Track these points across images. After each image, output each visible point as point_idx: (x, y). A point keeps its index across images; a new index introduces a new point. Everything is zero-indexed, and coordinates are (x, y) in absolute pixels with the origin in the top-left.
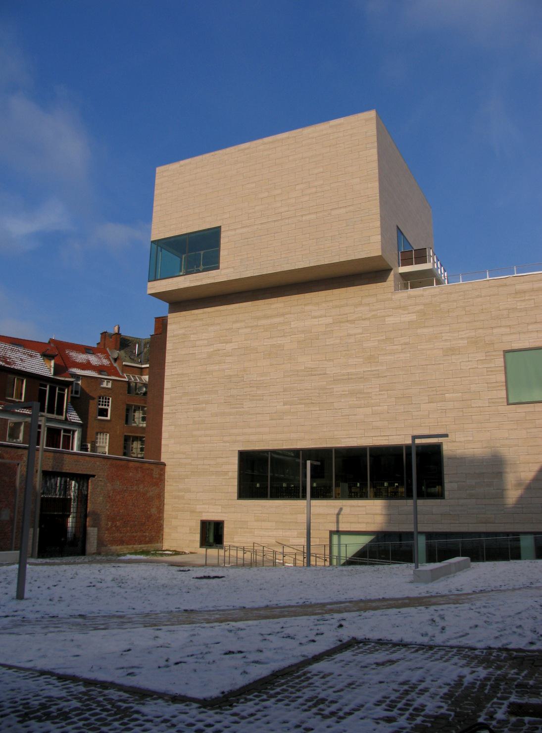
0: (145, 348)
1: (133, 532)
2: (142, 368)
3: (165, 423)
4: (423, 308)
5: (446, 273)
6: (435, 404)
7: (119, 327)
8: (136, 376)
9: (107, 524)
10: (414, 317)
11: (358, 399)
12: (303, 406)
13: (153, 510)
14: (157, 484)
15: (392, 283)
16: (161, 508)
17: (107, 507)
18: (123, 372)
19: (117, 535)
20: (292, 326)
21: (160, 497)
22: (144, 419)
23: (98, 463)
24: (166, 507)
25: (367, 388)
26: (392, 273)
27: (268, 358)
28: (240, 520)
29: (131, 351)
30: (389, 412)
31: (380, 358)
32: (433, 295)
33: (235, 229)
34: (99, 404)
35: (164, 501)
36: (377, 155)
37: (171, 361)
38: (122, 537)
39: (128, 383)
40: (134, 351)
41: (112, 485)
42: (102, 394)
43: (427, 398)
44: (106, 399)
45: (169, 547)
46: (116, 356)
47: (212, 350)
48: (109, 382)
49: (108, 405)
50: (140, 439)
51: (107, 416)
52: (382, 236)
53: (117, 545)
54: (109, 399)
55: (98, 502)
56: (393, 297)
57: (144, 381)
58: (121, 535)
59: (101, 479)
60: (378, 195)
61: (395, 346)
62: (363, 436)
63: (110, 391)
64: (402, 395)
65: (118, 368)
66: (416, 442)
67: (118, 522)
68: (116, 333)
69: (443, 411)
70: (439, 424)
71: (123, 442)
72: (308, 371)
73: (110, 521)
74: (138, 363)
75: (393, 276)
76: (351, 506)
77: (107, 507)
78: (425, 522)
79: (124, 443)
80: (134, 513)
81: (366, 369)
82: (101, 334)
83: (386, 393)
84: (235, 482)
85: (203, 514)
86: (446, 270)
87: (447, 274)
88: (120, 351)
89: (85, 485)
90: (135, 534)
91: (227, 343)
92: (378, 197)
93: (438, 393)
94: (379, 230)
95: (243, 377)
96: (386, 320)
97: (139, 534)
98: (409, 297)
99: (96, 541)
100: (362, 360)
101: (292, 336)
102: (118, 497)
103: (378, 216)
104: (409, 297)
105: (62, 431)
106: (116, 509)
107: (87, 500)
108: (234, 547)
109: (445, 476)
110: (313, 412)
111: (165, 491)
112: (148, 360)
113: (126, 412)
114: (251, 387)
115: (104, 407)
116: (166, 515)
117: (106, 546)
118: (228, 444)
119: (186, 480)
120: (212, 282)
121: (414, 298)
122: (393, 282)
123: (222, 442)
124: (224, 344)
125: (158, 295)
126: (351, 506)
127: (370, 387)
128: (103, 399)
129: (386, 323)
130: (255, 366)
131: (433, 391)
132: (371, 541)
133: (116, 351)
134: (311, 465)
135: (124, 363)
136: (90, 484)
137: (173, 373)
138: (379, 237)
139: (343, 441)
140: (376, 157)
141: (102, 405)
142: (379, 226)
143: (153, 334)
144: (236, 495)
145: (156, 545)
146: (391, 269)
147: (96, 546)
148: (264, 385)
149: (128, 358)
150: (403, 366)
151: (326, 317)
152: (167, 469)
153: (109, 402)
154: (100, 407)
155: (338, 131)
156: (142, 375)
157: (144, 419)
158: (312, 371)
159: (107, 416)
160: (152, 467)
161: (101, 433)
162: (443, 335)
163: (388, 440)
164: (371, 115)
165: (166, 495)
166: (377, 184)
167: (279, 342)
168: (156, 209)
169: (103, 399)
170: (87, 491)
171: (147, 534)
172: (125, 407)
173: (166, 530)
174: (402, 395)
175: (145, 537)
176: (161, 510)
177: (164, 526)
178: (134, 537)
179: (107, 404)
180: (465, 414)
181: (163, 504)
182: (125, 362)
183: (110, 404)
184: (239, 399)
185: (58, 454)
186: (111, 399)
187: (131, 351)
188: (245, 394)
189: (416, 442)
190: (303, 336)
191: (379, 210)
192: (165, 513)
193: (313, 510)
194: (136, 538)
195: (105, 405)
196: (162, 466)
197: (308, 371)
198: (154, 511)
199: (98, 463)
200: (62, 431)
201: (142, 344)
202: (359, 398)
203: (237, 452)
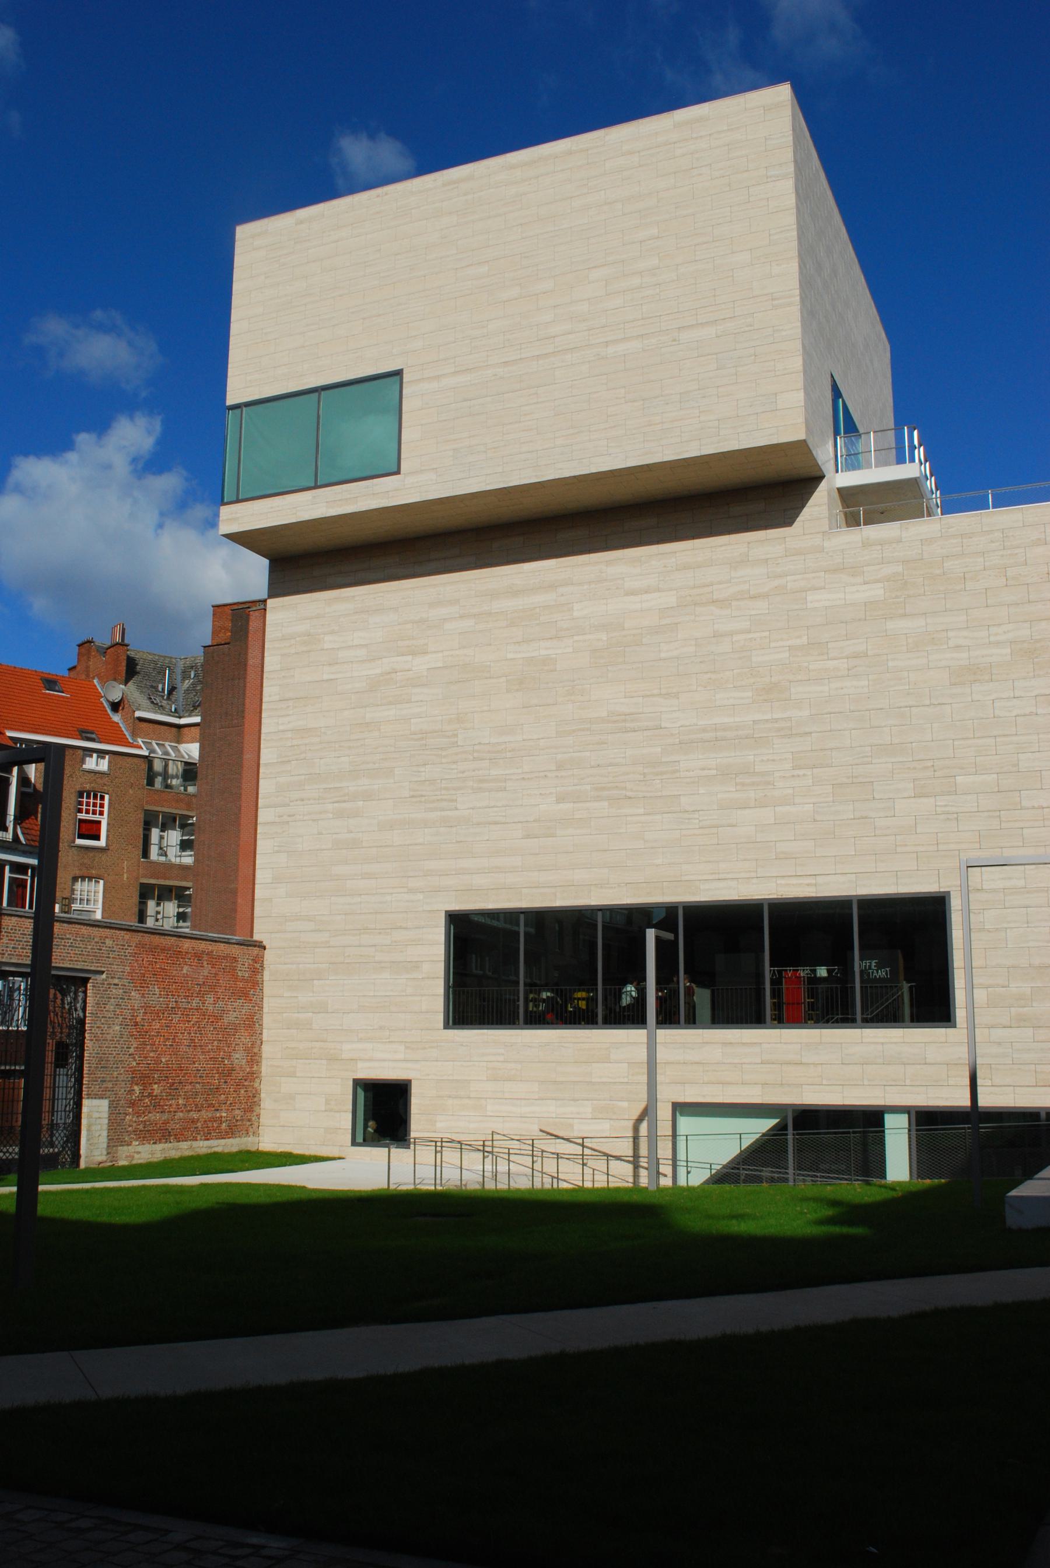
0: (184, 679)
1: (189, 1111)
2: (179, 727)
3: (264, 846)
4: (900, 569)
5: (938, 492)
6: (932, 800)
7: (124, 630)
8: (167, 744)
9: (131, 1092)
10: (877, 592)
11: (738, 788)
12: (606, 804)
13: (237, 1056)
14: (244, 994)
15: (824, 511)
16: (256, 1050)
17: (132, 1050)
18: (134, 735)
19: (155, 1117)
20: (576, 614)
21: (252, 1023)
22: (185, 845)
23: (109, 942)
24: (267, 1050)
25: (762, 761)
26: (823, 485)
27: (517, 690)
28: (451, 1078)
29: (152, 687)
30: (818, 818)
31: (793, 690)
32: (926, 540)
33: (438, 378)
34: (80, 811)
35: (261, 1034)
36: (794, 195)
37: (277, 698)
38: (166, 1123)
39: (149, 760)
40: (160, 687)
41: (143, 996)
42: (88, 787)
43: (912, 785)
44: (95, 797)
45: (276, 1145)
46: (116, 695)
47: (378, 671)
48: (104, 758)
49: (101, 813)
50: (179, 895)
51: (97, 837)
52: (805, 392)
53: (155, 1143)
54: (102, 798)
55: (109, 1037)
56: (826, 544)
57: (187, 757)
58: (165, 1116)
59: (116, 981)
60: (797, 292)
61: (830, 662)
62: (753, 875)
63: (106, 780)
64: (848, 778)
65: (121, 725)
66: (648, 931)
67: (156, 1086)
68: (117, 644)
69: (950, 816)
70: (941, 847)
71: (136, 899)
72: (615, 722)
73: (137, 1084)
74: (170, 714)
75: (826, 493)
76: (725, 1044)
77: (132, 1050)
78: (908, 1082)
79: (140, 902)
80: (194, 1063)
81: (758, 717)
82: (79, 646)
83: (809, 772)
84: (438, 988)
85: (360, 1065)
86: (938, 488)
87: (940, 493)
88: (126, 684)
89: (81, 995)
90: (194, 1115)
91: (413, 654)
92: (798, 298)
93: (937, 774)
94: (799, 380)
95: (456, 736)
96: (809, 598)
97: (206, 1114)
98: (866, 544)
99: (105, 1133)
100: (750, 694)
101: (576, 638)
102: (156, 1025)
103: (798, 345)
104: (866, 544)
105: (7, 868)
106: (152, 1054)
107: (83, 1031)
108: (452, 1141)
109: (955, 971)
110: (629, 818)
111: (265, 1010)
112: (195, 707)
113: (145, 829)
114: (475, 759)
115: (90, 817)
116: (266, 1068)
117: (128, 1145)
118: (421, 896)
119: (315, 982)
120: (381, 506)
121: (879, 547)
122: (825, 507)
123: (406, 890)
124: (410, 658)
125: (246, 539)
126: (725, 1044)
127: (768, 760)
128: (88, 797)
129: (810, 605)
130: (486, 708)
131: (926, 768)
132: (770, 1129)
133: (115, 683)
134: (658, 940)
135: (138, 714)
136: (89, 993)
137: (281, 728)
138: (801, 395)
139: (702, 887)
140: (791, 200)
141: (87, 812)
142: (801, 368)
143: (210, 643)
144: (440, 1017)
145: (244, 1140)
146: (821, 477)
147: (105, 1145)
148: (509, 755)
149: (144, 701)
150: (852, 708)
151: (659, 590)
152: (269, 956)
153: (102, 806)
154: (82, 816)
155: (694, 135)
156: (179, 742)
157: (185, 845)
158: (625, 721)
159: (97, 837)
160: (236, 950)
161: (83, 878)
162: (951, 634)
163: (815, 885)
164: (784, 92)
165: (267, 1020)
166: (794, 266)
167: (543, 652)
168: (235, 328)
169: (88, 797)
170: (84, 1010)
171: (224, 1115)
172: (142, 816)
173: (267, 1103)
174: (848, 778)
175: (220, 1120)
176: (254, 1057)
177: (263, 1095)
178: (193, 1121)
179: (98, 809)
180: (1004, 825)
181: (259, 1042)
182: (139, 710)
183: (106, 809)
184: (446, 789)
185: (14, 919)
186: (107, 797)
187: (152, 687)
188: (460, 775)
189: (648, 931)
190: (605, 639)
191: (799, 330)
192: (264, 1063)
193: (662, 1054)
194: (199, 1125)
195: (94, 813)
196: (256, 951)
197: (615, 722)
198: (239, 1058)
199: (109, 942)
200: (7, 868)
201: (179, 671)
202: (743, 784)
203: (443, 915)
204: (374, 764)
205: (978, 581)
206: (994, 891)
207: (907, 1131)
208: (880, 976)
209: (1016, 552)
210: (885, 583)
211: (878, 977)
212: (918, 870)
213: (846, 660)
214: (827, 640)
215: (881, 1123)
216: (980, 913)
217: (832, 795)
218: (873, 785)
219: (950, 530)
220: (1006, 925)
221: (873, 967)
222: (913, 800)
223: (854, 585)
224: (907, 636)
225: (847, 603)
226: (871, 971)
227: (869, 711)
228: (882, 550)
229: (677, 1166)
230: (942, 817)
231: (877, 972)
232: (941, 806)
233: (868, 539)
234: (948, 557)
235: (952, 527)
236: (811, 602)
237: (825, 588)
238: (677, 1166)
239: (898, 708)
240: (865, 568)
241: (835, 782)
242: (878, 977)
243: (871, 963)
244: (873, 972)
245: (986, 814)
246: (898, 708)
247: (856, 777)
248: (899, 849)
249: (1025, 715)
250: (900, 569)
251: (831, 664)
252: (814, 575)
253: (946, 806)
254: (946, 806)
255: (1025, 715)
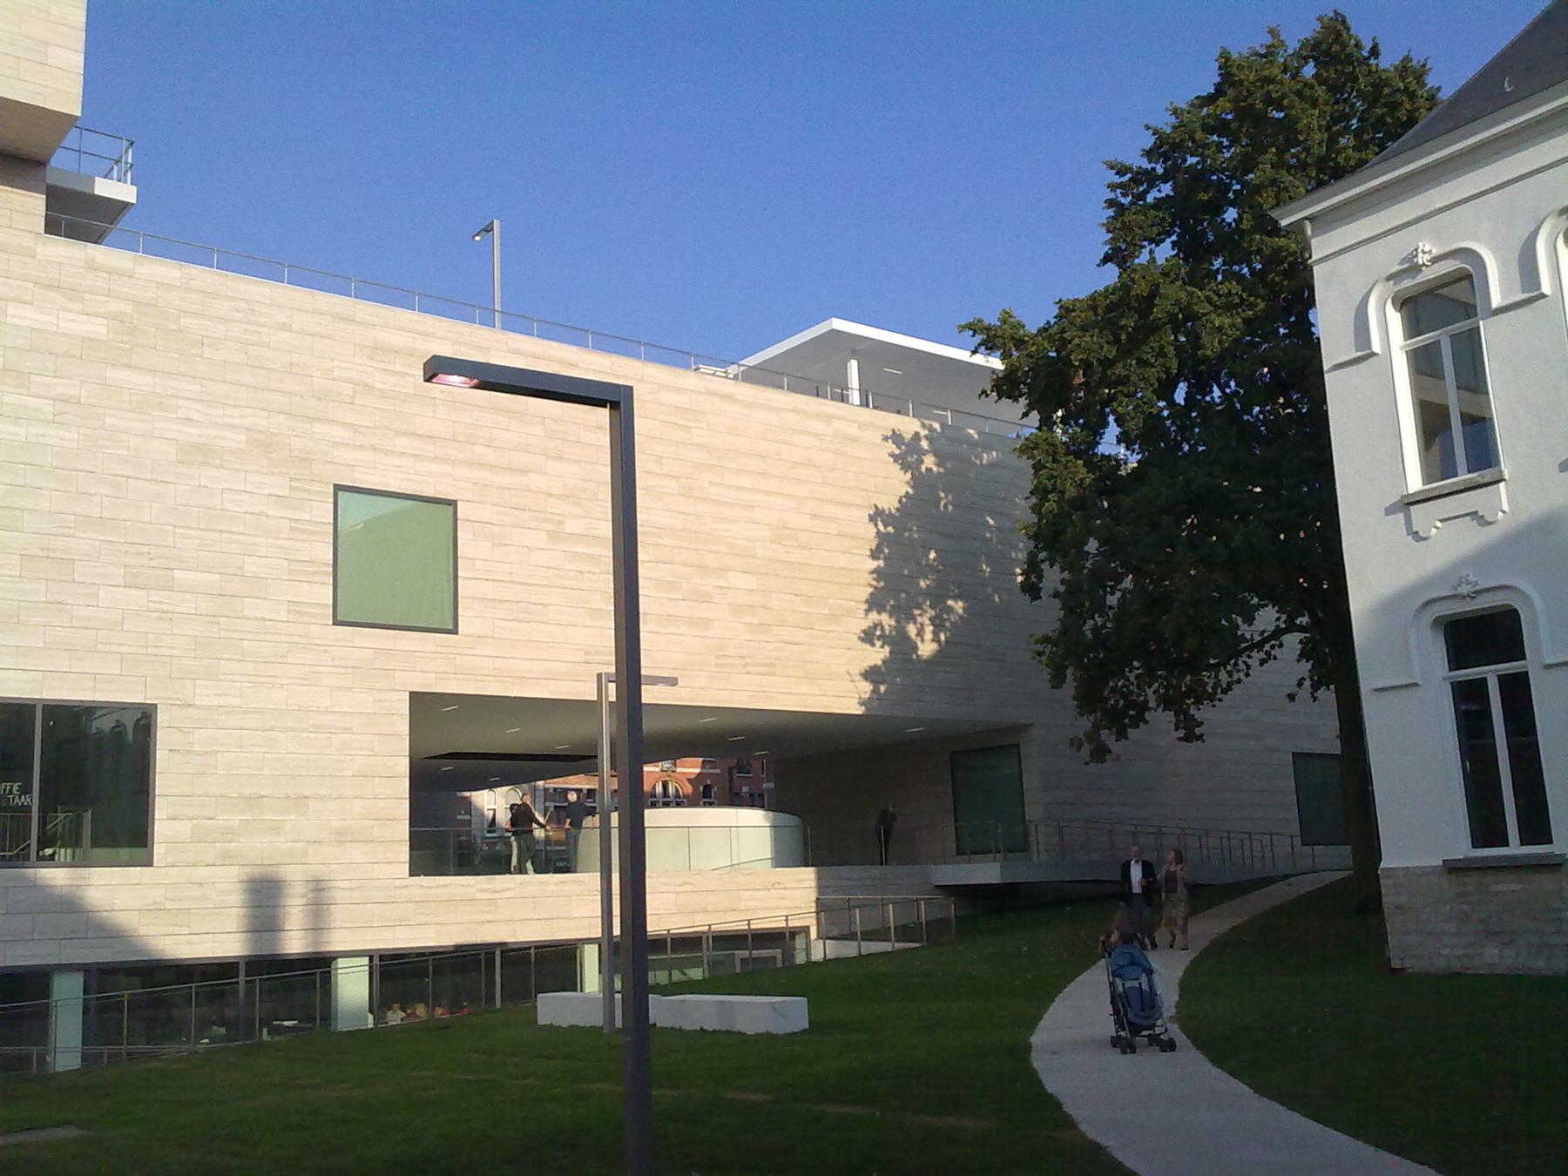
4: (129, 309)
6: (143, 593)
10: (99, 329)
69: (163, 615)
96: (10, 311)
98: (91, 266)
121: (106, 275)
131: (140, 554)
204: (126, 552)
205: (217, 350)
206: (207, 708)
207: (367, 968)
208: (23, 803)
209: (261, 330)
210: (110, 321)
211: (20, 804)
212: (121, 675)
213: (52, 402)
214: (30, 371)
215: (45, 991)
216: (189, 732)
217: (19, 568)
218: (74, 563)
219: (191, 282)
220: (215, 748)
221: (15, 792)
222: (121, 589)
223: (70, 312)
224: (55, 372)
225: (60, 331)
226: (11, 796)
227: (77, 471)
228: (109, 279)
229: (860, 955)
230: (156, 615)
231: (20, 798)
232: (154, 602)
233: (93, 260)
234: (185, 312)
235: (194, 280)
236: (13, 317)
237: (32, 304)
238: (860, 955)
239: (112, 475)
240: (86, 294)
241: (23, 553)
242: (20, 804)
243: (12, 786)
244: (13, 798)
245: (205, 618)
246: (112, 475)
247: (53, 550)
248: (100, 647)
249: (253, 514)
250: (129, 309)
251: (32, 402)
252: (18, 283)
253: (161, 602)
254: (161, 602)
255: (253, 514)
